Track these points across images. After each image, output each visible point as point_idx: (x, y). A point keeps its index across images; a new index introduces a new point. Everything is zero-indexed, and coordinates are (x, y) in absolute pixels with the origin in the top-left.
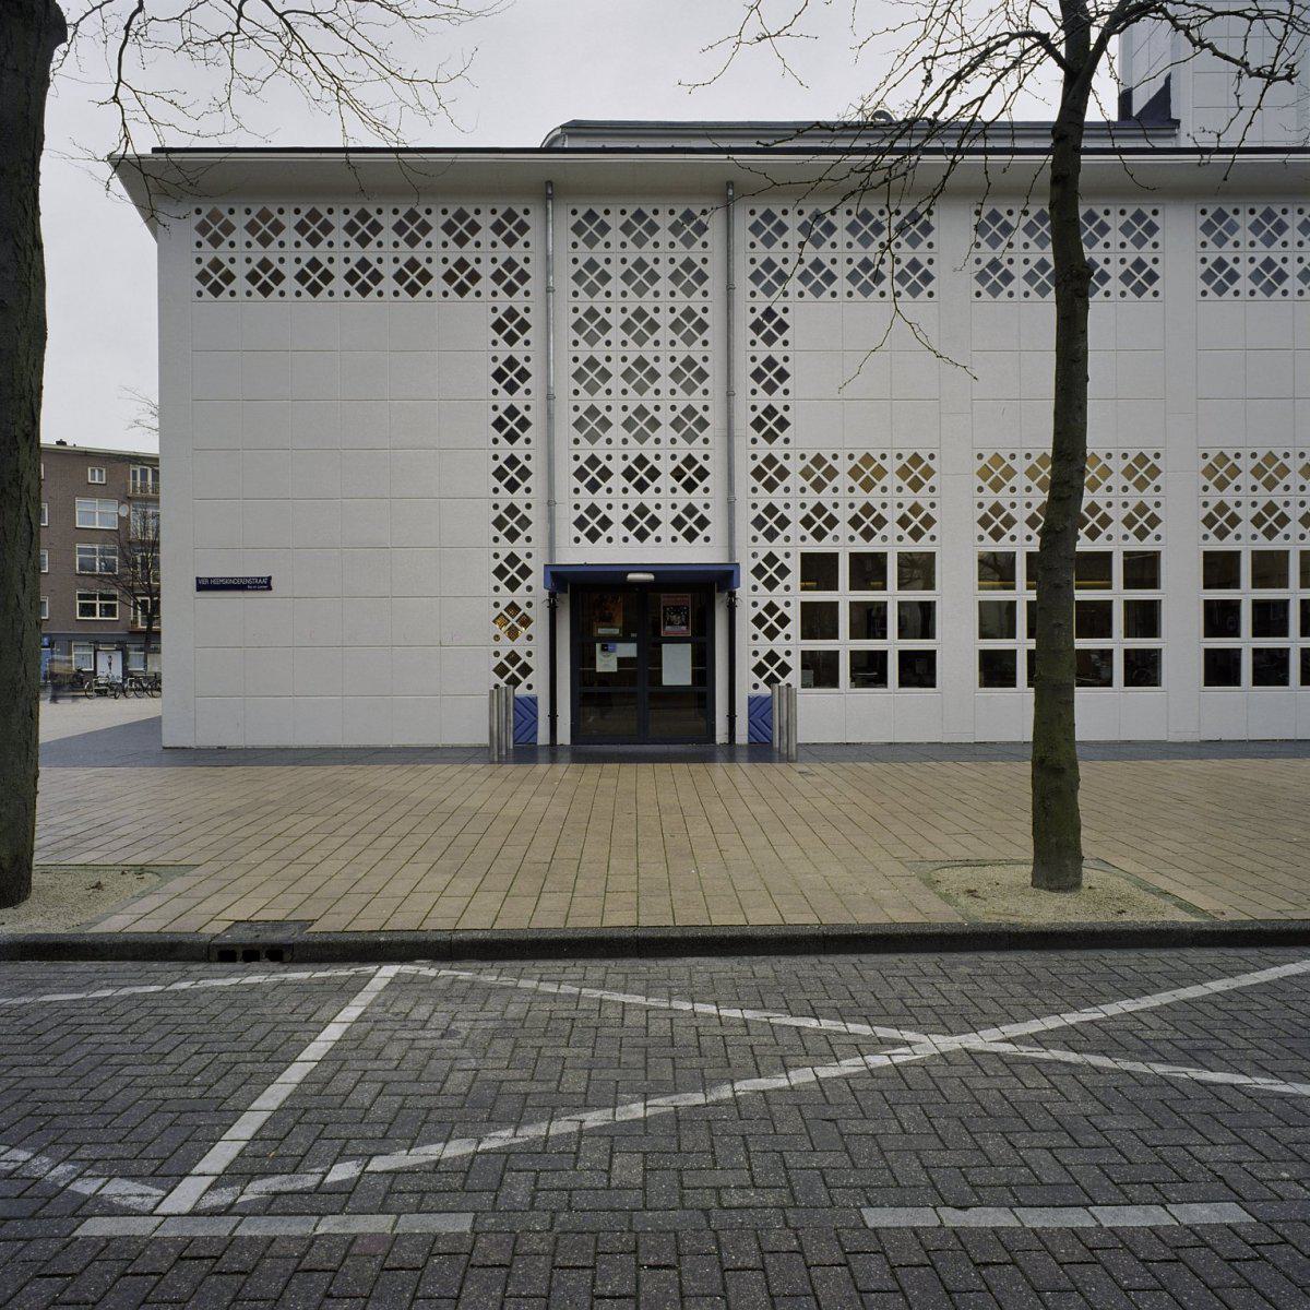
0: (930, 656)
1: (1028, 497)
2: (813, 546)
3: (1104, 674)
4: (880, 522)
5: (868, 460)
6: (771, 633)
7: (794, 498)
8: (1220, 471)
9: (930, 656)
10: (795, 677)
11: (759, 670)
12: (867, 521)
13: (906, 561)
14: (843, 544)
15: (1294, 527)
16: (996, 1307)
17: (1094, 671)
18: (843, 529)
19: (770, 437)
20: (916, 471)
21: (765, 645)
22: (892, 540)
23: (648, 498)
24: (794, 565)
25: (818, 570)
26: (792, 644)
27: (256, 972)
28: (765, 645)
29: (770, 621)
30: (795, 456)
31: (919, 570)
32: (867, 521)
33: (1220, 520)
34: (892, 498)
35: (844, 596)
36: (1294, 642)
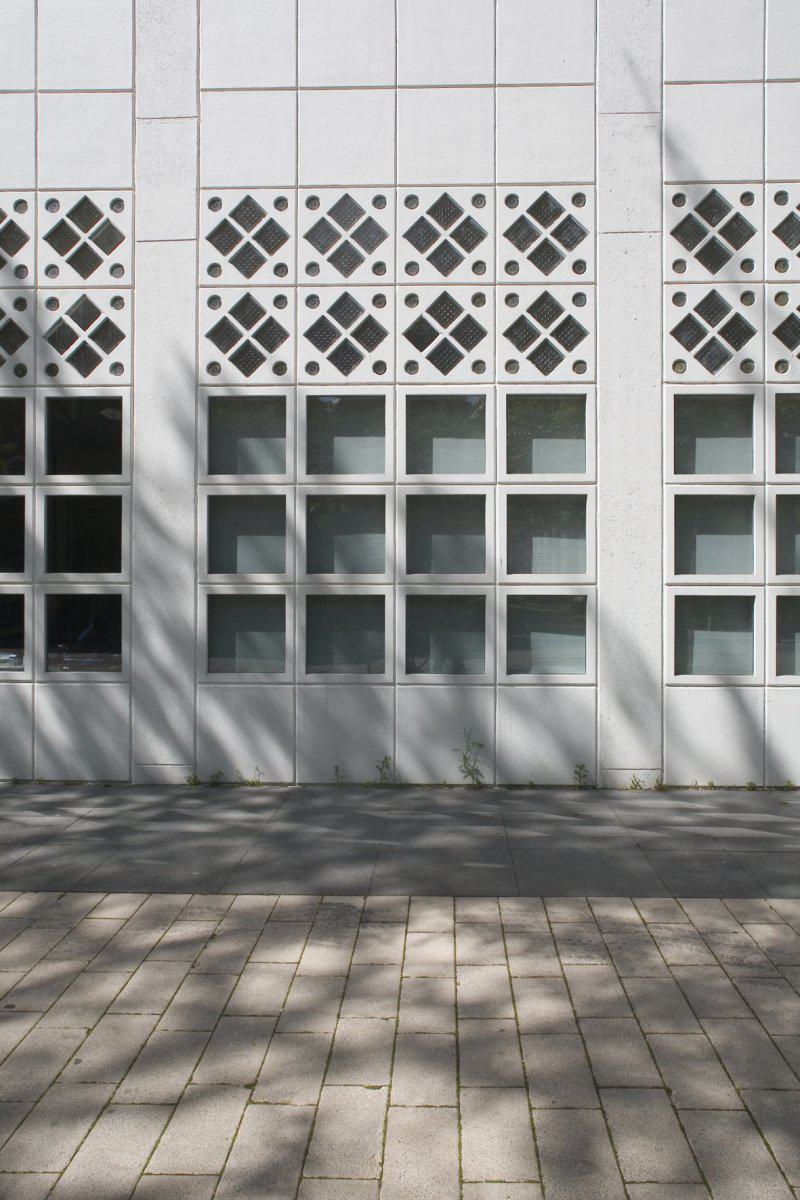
3: (580, 599)
8: (247, 235)
15: (763, 349)
16: (625, 1198)
20: (549, 229)
27: (235, 820)
33: (245, 333)
34: (496, 283)
36: (35, 492)
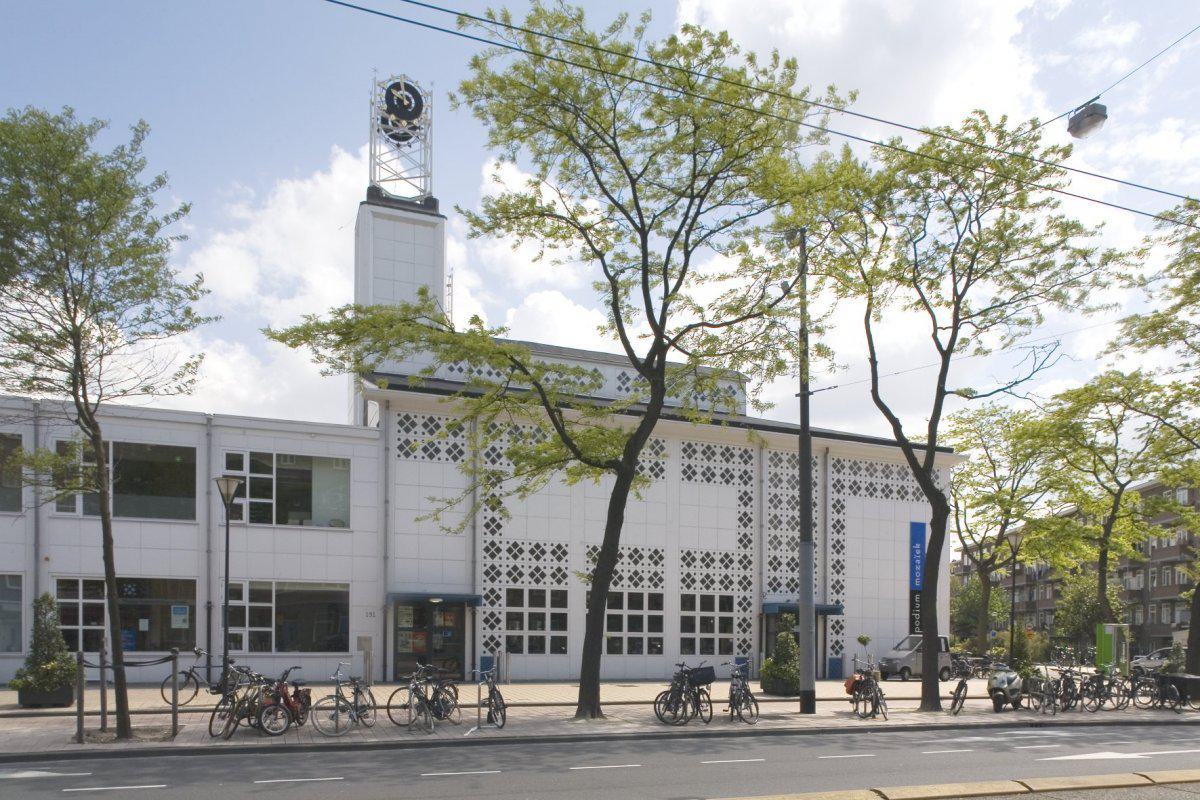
0: (660, 640)
1: (623, 567)
2: (512, 585)
4: (543, 575)
5: (636, 551)
6: (492, 627)
7: (504, 562)
8: (688, 558)
9: (564, 639)
10: (503, 648)
11: (486, 644)
12: (537, 574)
13: (554, 593)
14: (526, 585)
17: (615, 647)
18: (526, 578)
19: (493, 532)
20: (560, 552)
21: (489, 633)
22: (717, 590)
23: (518, 563)
24: (503, 594)
25: (515, 597)
26: (502, 632)
28: (489, 633)
29: (492, 621)
30: (504, 543)
31: (657, 601)
32: (537, 574)
33: (688, 580)
34: (548, 564)
35: (526, 610)
